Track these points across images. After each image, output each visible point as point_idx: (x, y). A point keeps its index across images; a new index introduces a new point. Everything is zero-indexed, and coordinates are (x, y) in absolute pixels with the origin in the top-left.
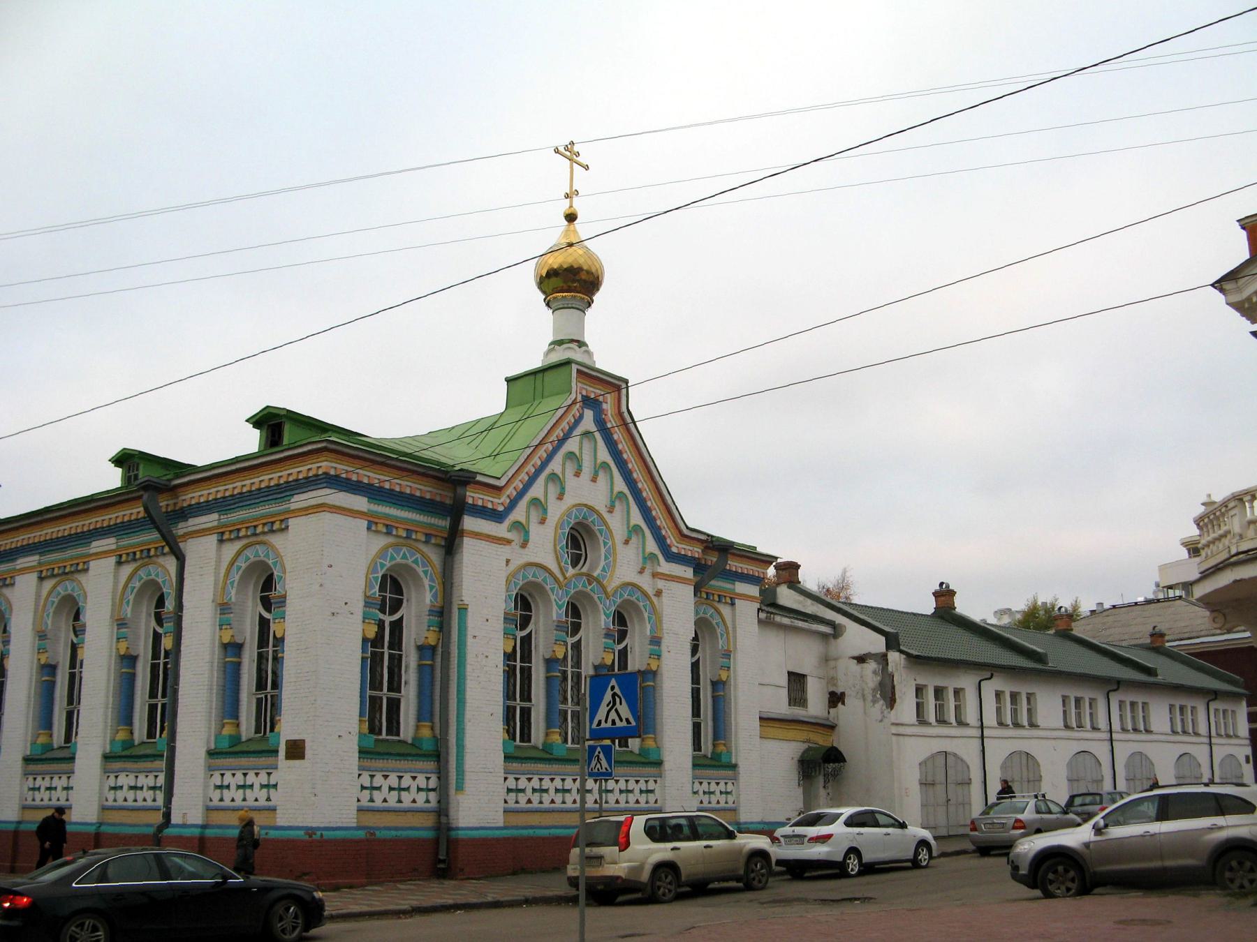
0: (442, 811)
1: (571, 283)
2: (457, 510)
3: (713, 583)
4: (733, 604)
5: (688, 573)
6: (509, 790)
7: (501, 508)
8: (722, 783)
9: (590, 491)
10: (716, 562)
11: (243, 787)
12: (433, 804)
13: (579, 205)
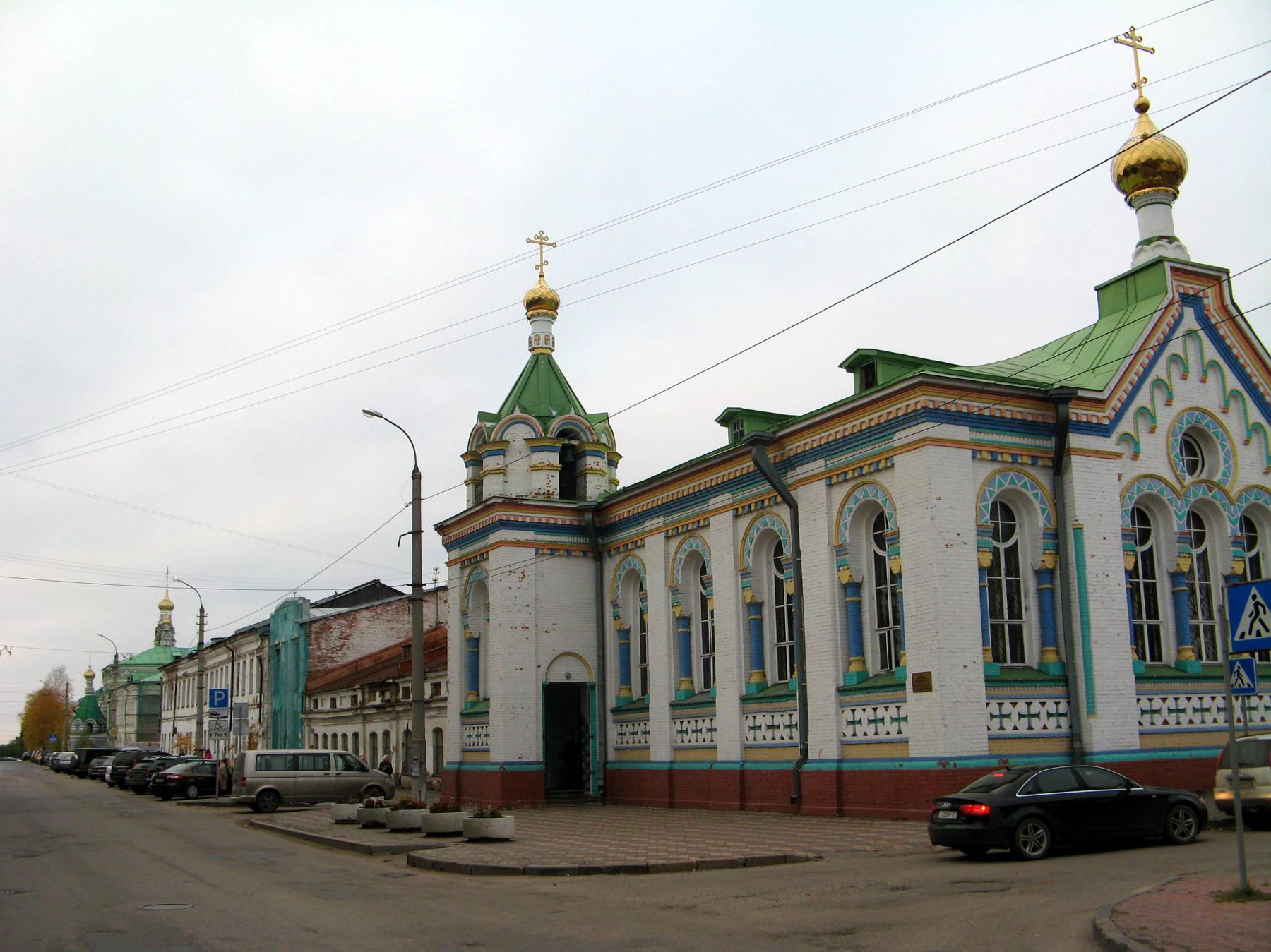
0: (1074, 736)
1: (1152, 177)
2: (1061, 429)
6: (1143, 712)
8: (1170, 698)
11: (633, 733)
12: (1065, 729)
13: (1148, 93)
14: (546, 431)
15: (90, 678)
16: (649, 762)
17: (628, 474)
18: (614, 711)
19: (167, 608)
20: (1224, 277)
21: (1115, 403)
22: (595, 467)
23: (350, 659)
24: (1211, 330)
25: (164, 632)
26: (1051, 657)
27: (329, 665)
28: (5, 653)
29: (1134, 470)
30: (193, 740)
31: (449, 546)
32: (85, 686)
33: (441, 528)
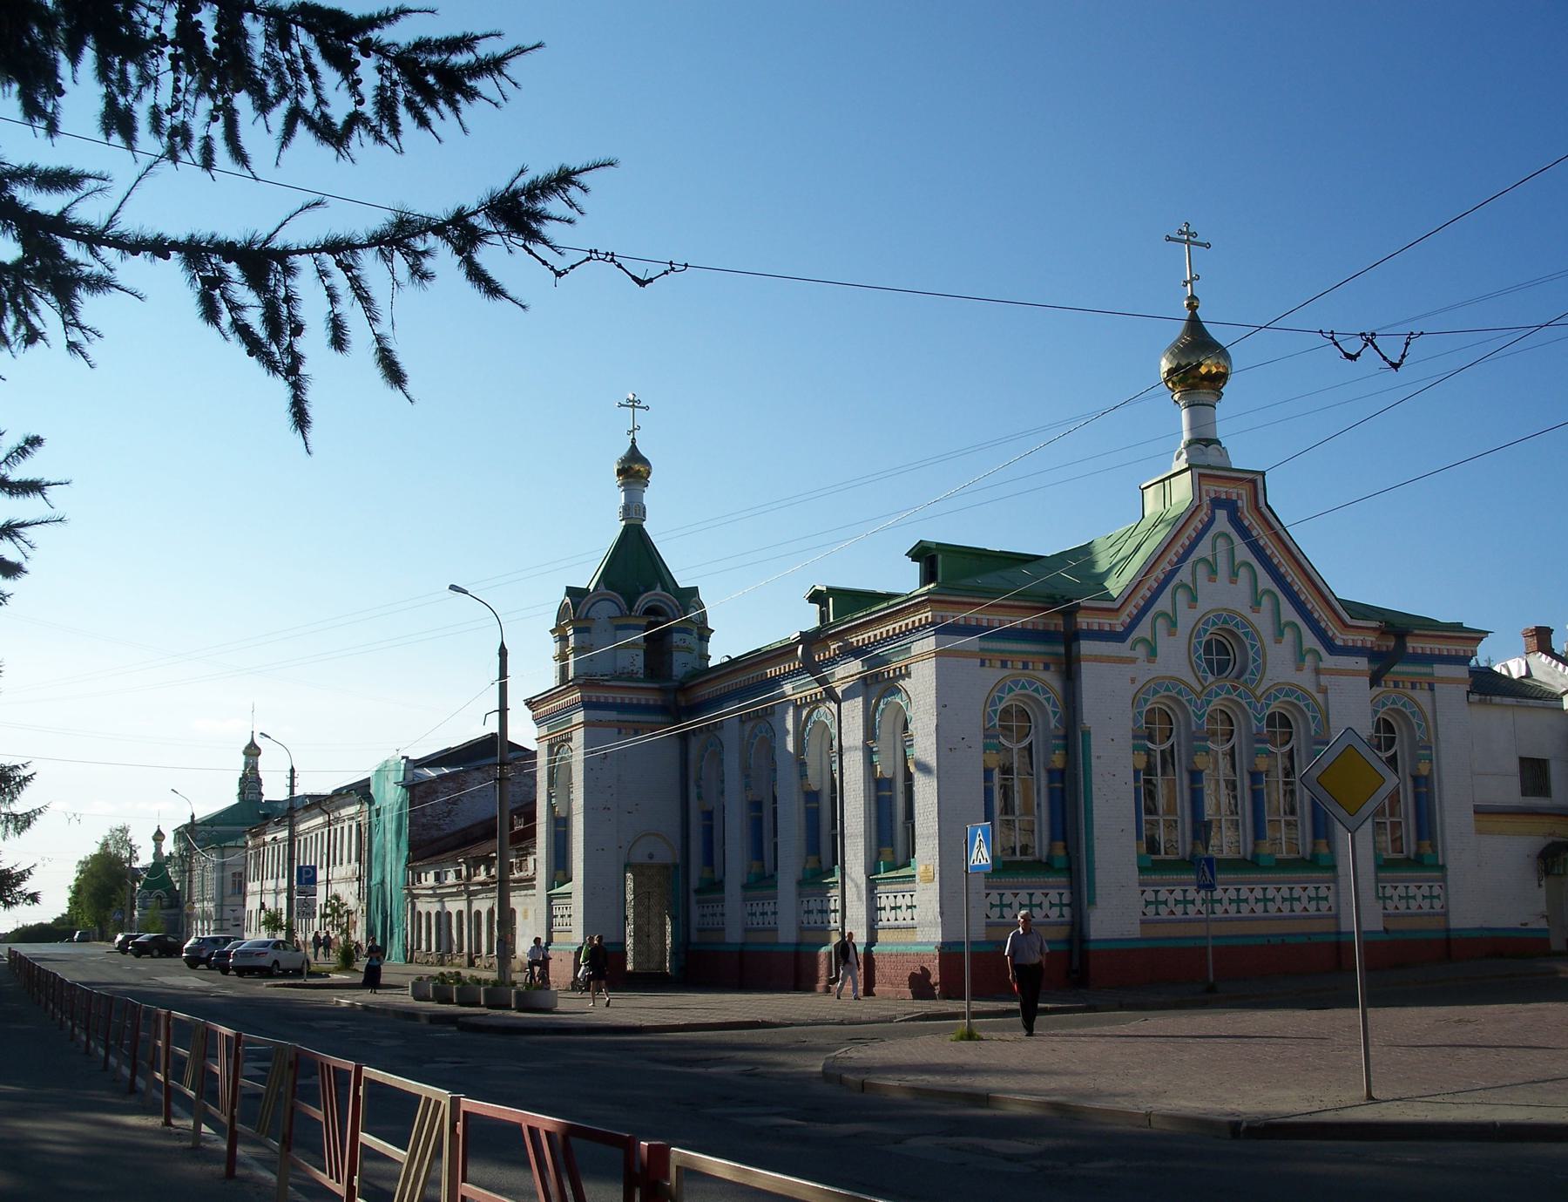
0: (1077, 925)
2: (1072, 636)
3: (1396, 668)
4: (1431, 689)
5: (1362, 663)
6: (1148, 903)
7: (1120, 629)
8: (1401, 886)
9: (1227, 594)
10: (1395, 642)
12: (1067, 917)
14: (631, 608)
15: (159, 837)
16: (777, 944)
17: (719, 651)
18: (698, 891)
19: (252, 751)
20: (1259, 478)
21: (1131, 609)
22: (681, 644)
23: (458, 827)
24: (1244, 532)
25: (250, 781)
26: (1059, 850)
27: (435, 834)
28: (74, 820)
29: (1145, 672)
30: (284, 917)
31: (538, 721)
32: (153, 850)
33: (530, 703)
